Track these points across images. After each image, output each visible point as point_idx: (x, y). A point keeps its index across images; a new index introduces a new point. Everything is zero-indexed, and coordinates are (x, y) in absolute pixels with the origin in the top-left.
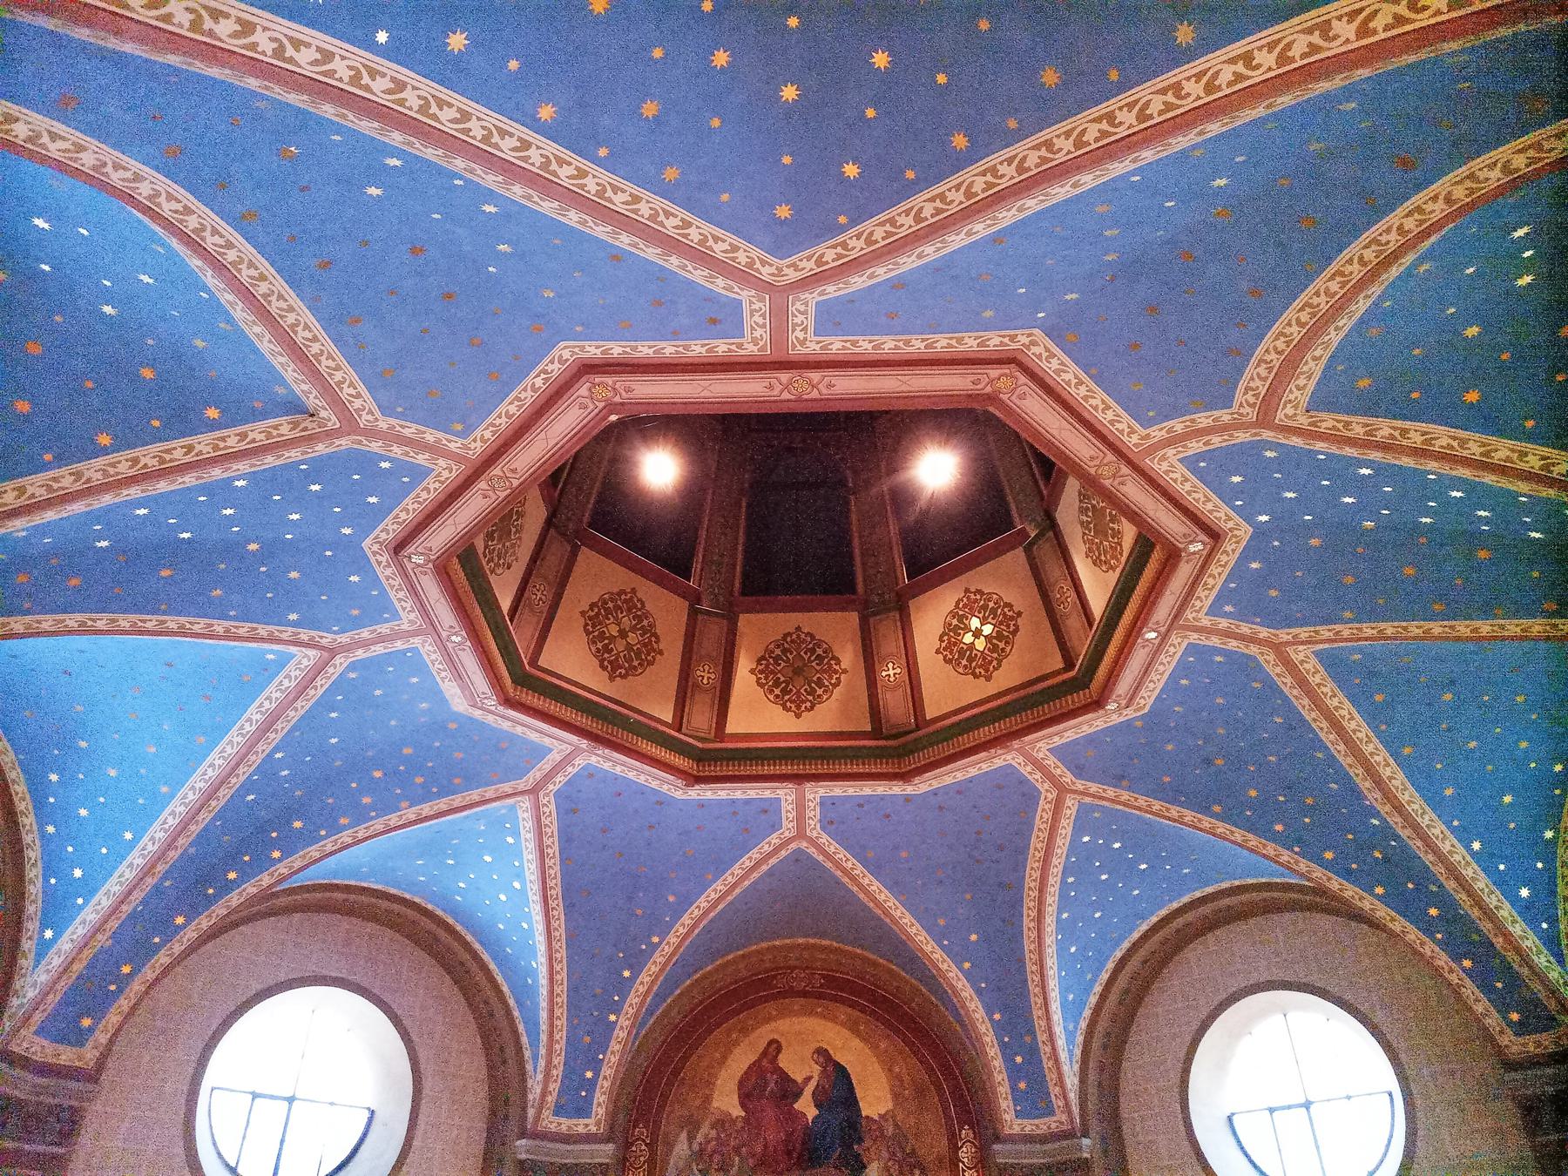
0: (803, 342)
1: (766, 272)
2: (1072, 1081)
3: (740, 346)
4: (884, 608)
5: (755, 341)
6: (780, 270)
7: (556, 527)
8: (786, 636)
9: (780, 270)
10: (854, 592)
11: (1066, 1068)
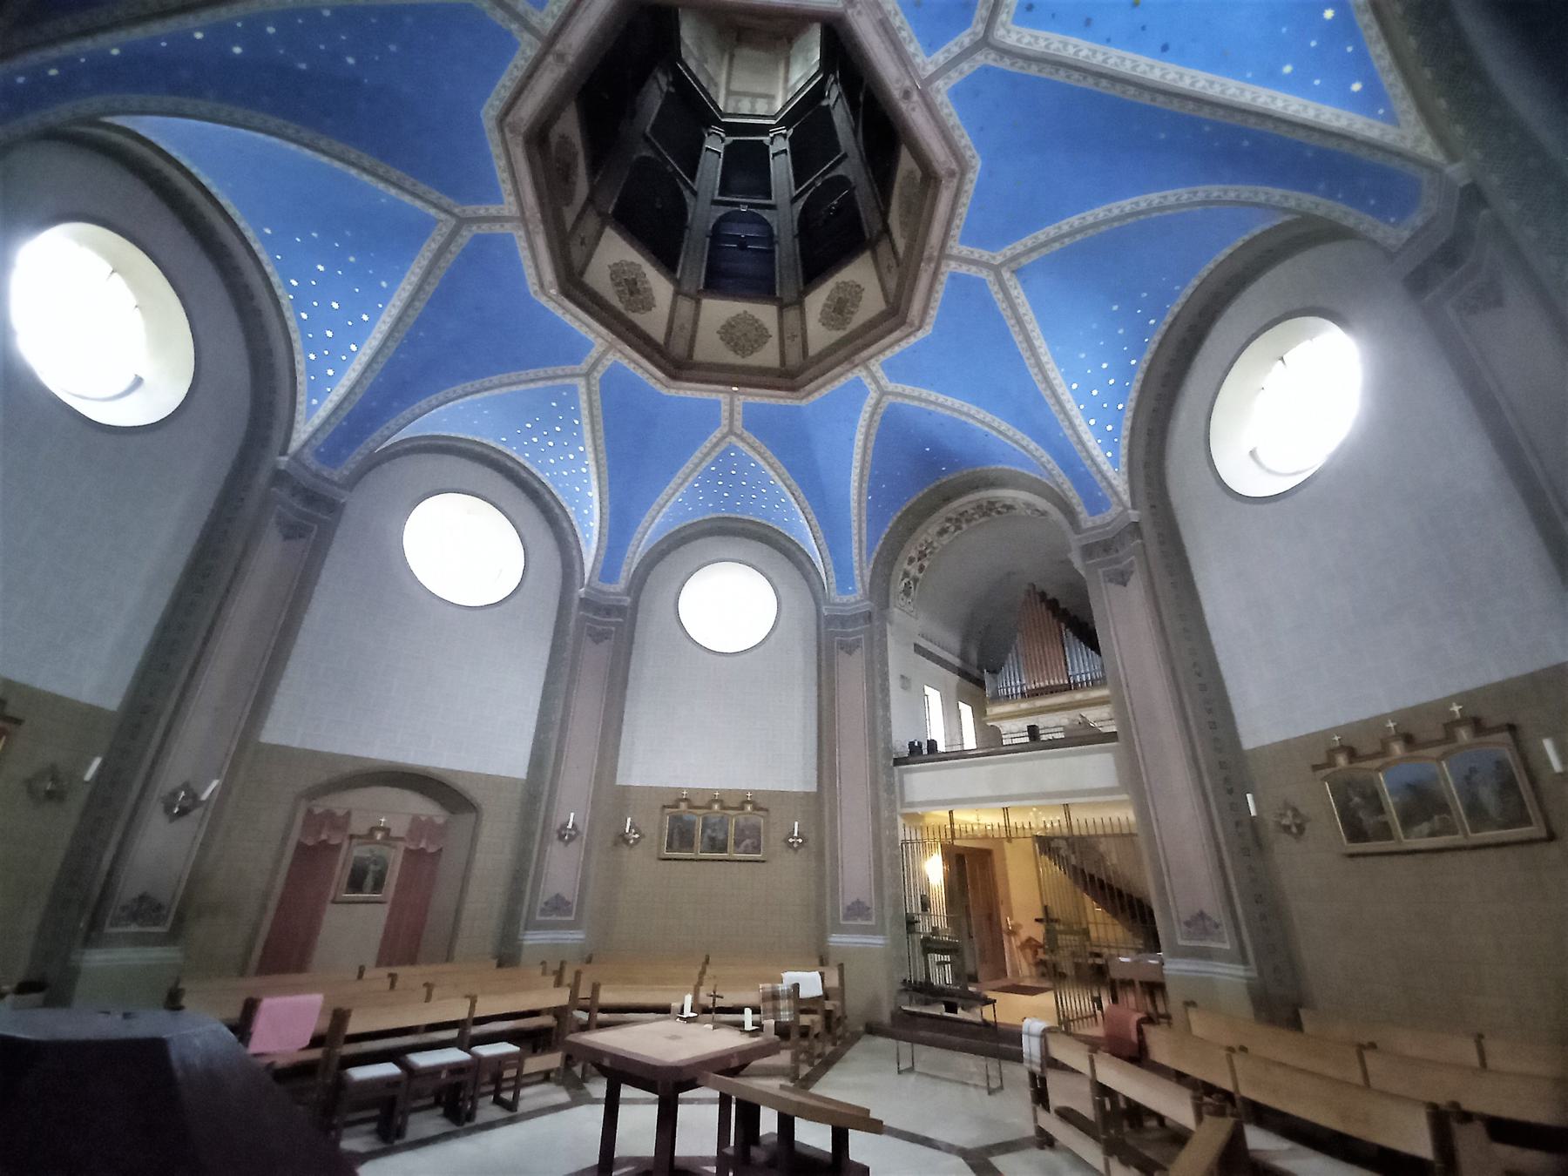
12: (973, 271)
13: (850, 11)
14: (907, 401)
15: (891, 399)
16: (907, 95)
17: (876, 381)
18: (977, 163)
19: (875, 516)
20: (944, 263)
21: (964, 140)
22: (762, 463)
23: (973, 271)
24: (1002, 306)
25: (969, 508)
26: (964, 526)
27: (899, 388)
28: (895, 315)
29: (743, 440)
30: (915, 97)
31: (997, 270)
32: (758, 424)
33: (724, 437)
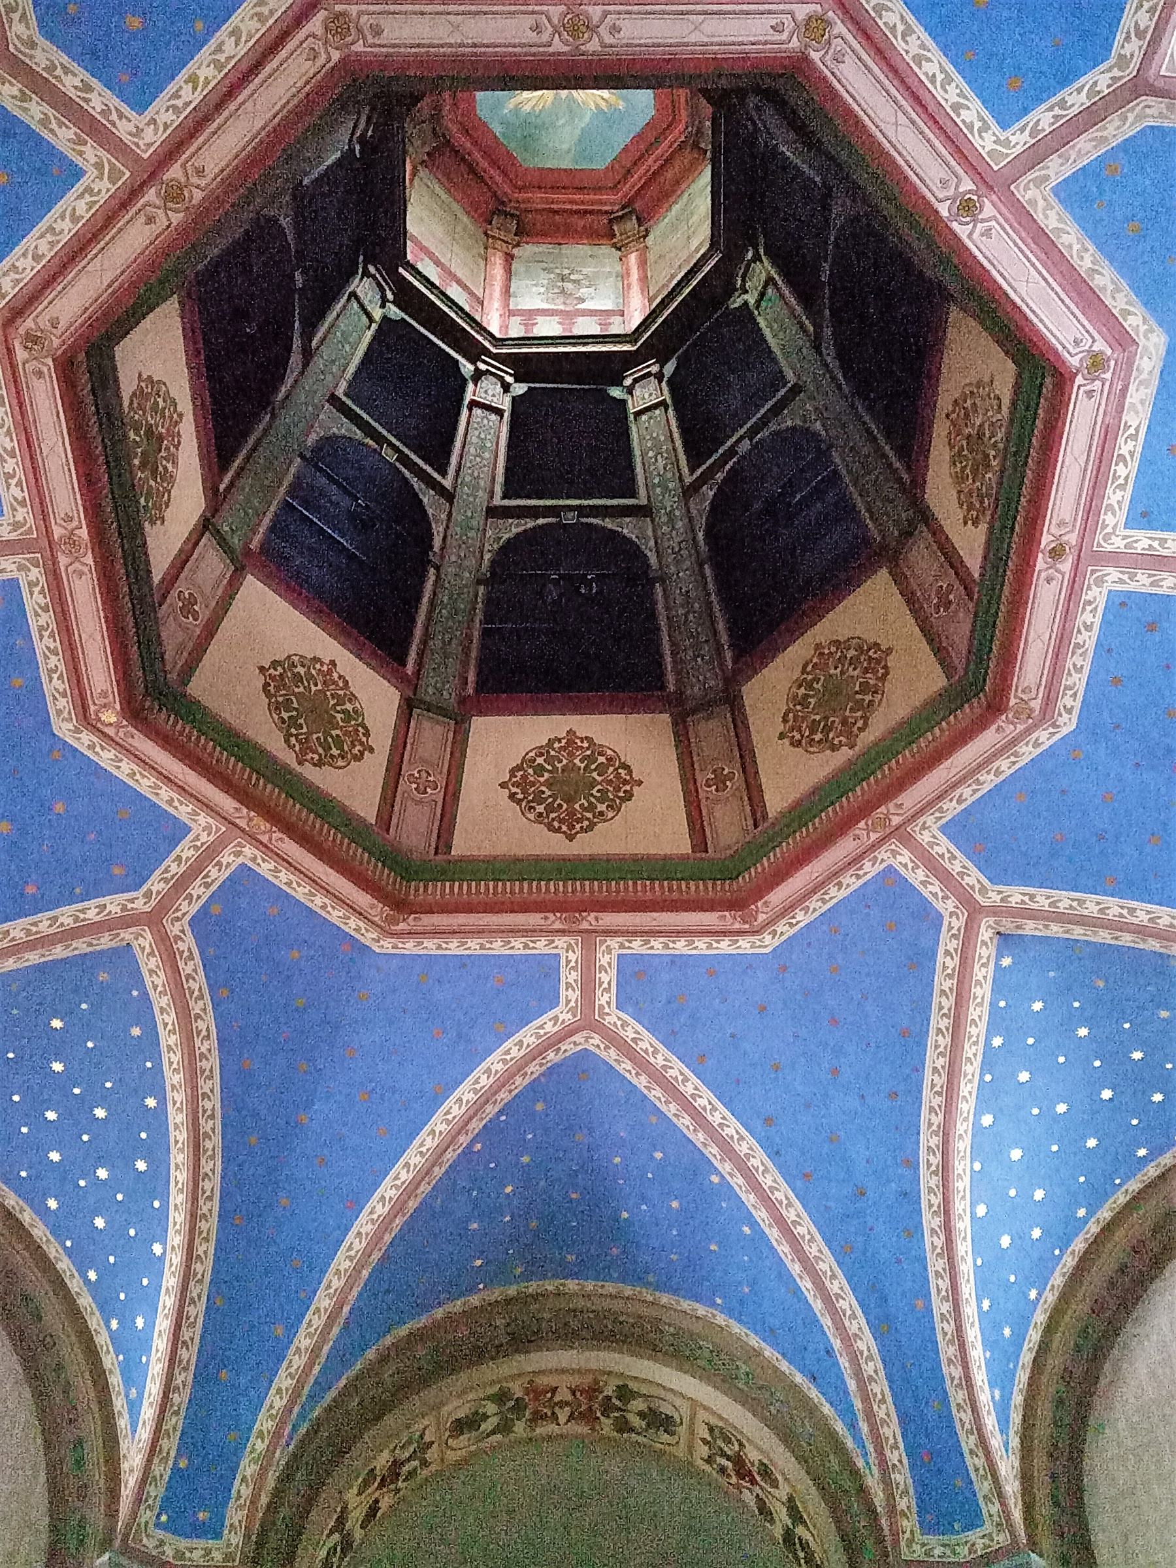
0: (569, 947)
1: (596, 1040)
2: (1008, 1467)
3: (622, 946)
4: (705, 706)
5: (609, 950)
6: (586, 1041)
7: (217, 533)
8: (591, 827)
9: (586, 1041)
10: (663, 687)
11: (995, 1443)
12: (933, 889)
13: (1079, 380)
14: (625, 1067)
15: (594, 1042)
16: (1057, 553)
17: (588, 986)
18: (1068, 724)
19: (361, 1322)
20: (893, 844)
21: (1077, 680)
22: (169, 1039)
23: (933, 889)
24: (943, 983)
25: (563, 1384)
26: (520, 1428)
27: (632, 1030)
28: (723, 875)
29: (171, 959)
30: (1066, 566)
31: (974, 911)
32: (236, 934)
33: (129, 920)
